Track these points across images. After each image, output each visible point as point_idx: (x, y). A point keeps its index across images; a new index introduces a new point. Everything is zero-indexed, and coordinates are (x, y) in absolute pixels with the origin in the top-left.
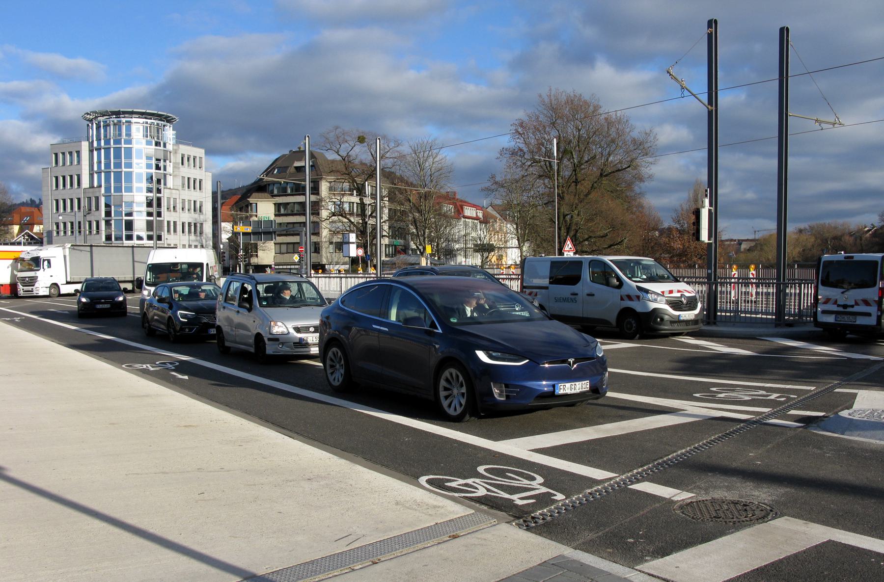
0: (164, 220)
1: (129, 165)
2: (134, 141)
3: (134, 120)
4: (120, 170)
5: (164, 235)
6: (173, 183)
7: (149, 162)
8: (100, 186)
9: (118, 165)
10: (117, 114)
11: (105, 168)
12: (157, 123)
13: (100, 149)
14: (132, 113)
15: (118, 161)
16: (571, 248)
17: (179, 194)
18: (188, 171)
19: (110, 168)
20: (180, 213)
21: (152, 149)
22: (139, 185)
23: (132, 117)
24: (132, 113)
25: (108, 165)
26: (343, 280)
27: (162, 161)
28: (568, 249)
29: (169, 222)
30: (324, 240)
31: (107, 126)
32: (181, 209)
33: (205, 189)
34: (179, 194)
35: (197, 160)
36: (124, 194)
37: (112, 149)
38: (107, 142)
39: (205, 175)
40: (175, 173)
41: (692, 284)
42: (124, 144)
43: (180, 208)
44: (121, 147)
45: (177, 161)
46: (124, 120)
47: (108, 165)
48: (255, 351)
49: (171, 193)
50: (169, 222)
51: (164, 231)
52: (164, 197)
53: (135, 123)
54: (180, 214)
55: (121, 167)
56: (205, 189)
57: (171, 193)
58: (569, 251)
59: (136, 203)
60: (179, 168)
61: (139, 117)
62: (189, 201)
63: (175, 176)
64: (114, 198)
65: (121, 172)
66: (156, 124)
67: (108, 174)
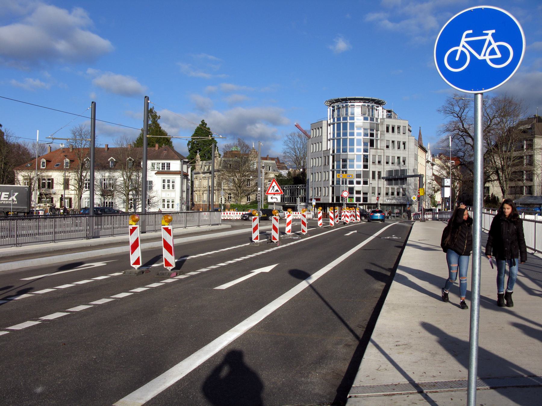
0: (369, 171)
1: (352, 134)
2: (355, 118)
3: (356, 104)
4: (339, 138)
5: (369, 181)
6: (380, 145)
7: (366, 132)
8: (330, 149)
9: (345, 134)
10: (346, 100)
11: (337, 136)
12: (372, 106)
13: (334, 124)
14: (355, 99)
15: (345, 131)
16: (277, 191)
17: (384, 153)
18: (390, 136)
19: (340, 136)
20: (384, 165)
21: (361, 122)
22: (359, 147)
23: (354, 102)
24: (355, 99)
25: (339, 135)
26: (94, 217)
27: (375, 130)
28: (272, 192)
29: (374, 173)
30: (536, 184)
31: (339, 108)
32: (385, 163)
33: (408, 148)
34: (384, 153)
35: (401, 129)
36: (349, 153)
37: (342, 124)
38: (339, 119)
39: (409, 139)
40: (382, 138)
41: (26, 219)
42: (350, 120)
43: (384, 162)
44: (347, 123)
45: (383, 130)
46: (350, 104)
47: (339, 135)
48: (385, 283)
49: (376, 152)
50: (374, 173)
51: (369, 178)
52: (370, 155)
53: (356, 106)
54: (384, 167)
55: (347, 136)
56: (408, 148)
57: (376, 152)
58: (274, 194)
59: (349, 159)
60: (384, 134)
61: (360, 102)
62: (398, 158)
63: (381, 140)
64: (336, 157)
65: (347, 139)
66: (371, 106)
67: (338, 141)
